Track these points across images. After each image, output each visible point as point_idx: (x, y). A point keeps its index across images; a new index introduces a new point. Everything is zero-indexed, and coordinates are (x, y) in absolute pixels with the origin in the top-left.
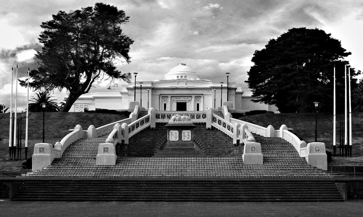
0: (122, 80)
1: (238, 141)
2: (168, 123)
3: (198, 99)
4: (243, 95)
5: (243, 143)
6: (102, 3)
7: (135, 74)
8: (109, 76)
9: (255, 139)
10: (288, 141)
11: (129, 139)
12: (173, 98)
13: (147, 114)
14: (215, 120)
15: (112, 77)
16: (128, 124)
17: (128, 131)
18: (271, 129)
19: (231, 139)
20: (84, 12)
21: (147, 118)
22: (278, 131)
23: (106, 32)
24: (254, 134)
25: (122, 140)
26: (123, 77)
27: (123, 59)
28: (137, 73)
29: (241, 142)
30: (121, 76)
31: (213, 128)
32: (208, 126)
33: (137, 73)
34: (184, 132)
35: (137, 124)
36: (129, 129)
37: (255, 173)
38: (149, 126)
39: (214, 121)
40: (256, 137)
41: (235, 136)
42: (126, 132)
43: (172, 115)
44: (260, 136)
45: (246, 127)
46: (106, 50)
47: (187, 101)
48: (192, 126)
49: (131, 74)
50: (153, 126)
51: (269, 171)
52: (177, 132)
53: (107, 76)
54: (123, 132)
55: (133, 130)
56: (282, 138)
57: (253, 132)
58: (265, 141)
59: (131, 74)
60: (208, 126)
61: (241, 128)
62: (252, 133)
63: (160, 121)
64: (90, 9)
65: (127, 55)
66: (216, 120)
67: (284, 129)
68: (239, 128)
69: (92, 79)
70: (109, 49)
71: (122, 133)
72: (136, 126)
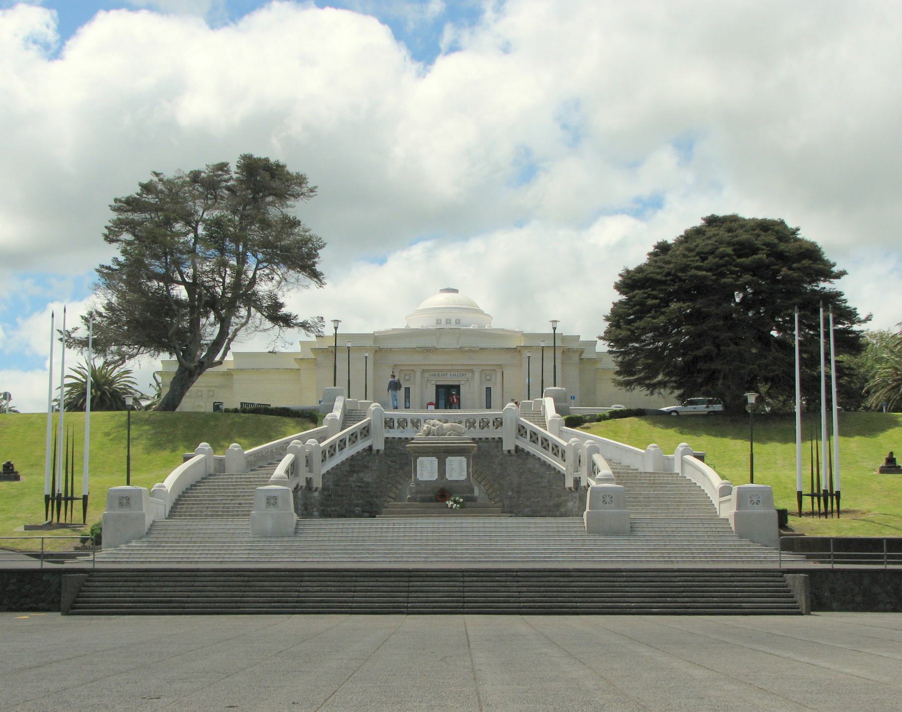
0: (303, 331)
1: (577, 481)
7: (336, 323)
10: (693, 481)
12: (427, 375)
14: (522, 431)
16: (321, 439)
17: (320, 457)
19: (561, 476)
23: (266, 224)
29: (583, 483)
32: (508, 445)
34: (450, 461)
36: (324, 452)
38: (370, 447)
39: (522, 435)
46: (265, 264)
47: (462, 382)
50: (379, 445)
52: (434, 461)
53: (268, 324)
60: (508, 445)
63: (396, 433)
64: (223, 167)
71: (307, 461)
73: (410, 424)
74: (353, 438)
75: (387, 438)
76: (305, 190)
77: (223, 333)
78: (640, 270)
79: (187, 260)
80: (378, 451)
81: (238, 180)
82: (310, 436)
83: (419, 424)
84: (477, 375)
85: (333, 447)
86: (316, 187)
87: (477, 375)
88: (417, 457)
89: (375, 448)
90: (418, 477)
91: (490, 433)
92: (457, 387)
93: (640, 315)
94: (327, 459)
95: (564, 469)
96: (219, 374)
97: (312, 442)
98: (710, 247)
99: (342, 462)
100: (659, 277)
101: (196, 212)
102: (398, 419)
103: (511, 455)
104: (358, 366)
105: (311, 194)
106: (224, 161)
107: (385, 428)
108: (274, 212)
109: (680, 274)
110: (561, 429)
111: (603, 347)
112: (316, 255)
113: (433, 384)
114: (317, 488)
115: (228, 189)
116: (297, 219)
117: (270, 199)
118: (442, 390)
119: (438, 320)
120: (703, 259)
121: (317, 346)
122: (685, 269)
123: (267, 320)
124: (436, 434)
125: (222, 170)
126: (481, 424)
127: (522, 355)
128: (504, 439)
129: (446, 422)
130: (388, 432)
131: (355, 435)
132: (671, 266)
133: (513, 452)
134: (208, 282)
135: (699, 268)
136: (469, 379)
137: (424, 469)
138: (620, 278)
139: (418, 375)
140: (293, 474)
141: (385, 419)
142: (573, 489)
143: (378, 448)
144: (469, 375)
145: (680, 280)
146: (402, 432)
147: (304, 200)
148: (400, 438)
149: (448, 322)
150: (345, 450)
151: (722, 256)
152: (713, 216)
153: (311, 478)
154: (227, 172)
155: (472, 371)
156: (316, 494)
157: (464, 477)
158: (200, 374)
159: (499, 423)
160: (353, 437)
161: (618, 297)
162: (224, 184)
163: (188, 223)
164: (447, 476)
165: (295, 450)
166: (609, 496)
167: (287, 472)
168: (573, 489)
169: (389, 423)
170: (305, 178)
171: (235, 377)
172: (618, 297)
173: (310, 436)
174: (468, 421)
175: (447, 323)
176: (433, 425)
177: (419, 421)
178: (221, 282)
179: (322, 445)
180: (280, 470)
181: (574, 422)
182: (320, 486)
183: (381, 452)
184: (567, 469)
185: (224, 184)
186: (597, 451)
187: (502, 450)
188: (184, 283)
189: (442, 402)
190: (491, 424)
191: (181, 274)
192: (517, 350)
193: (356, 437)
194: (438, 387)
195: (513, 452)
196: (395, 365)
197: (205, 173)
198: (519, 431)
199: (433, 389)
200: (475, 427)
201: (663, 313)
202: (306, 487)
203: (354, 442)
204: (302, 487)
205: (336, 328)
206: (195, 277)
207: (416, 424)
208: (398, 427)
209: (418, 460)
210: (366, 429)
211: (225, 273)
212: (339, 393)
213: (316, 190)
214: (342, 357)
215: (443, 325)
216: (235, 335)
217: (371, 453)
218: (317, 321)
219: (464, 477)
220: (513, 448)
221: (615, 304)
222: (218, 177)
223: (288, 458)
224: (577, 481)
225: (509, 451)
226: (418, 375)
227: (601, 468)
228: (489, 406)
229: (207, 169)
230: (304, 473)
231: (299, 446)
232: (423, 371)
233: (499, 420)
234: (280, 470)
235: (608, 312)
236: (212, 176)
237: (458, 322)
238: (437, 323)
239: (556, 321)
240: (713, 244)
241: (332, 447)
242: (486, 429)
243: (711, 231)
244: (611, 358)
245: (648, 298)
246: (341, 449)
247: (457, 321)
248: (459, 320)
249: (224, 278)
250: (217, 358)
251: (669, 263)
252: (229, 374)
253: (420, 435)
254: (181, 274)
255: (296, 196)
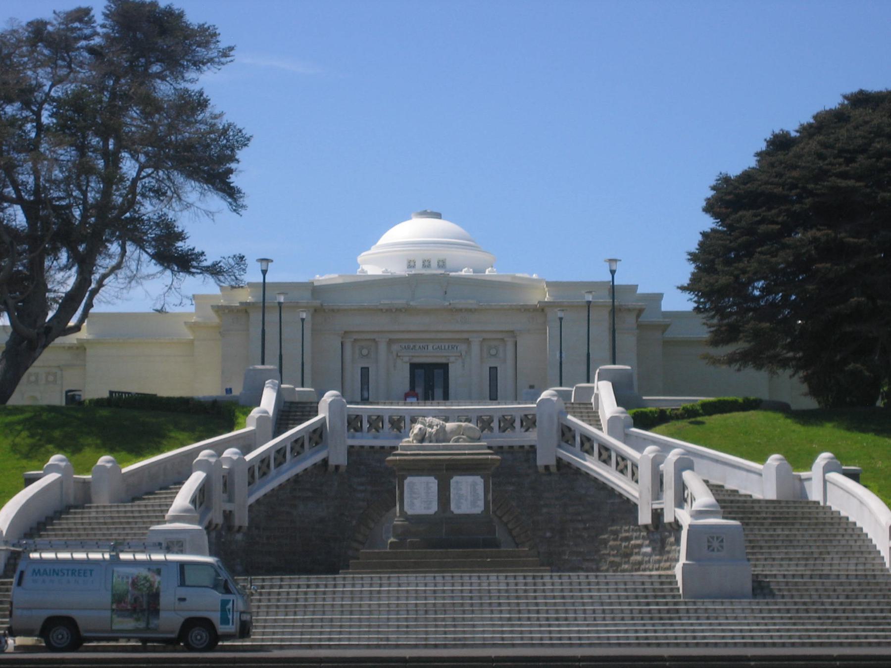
0: (210, 280)
1: (657, 515)
2: (395, 448)
3: (365, 352)
4: (669, 335)
5: (676, 521)
6: (818, 114)
7: (264, 263)
8: (159, 268)
9: (722, 507)
10: (843, 514)
11: (250, 506)
12: (395, 347)
13: (316, 413)
14: (568, 435)
15: (173, 271)
16: (247, 449)
17: (246, 478)
18: (778, 468)
19: (629, 508)
20: (60, 24)
21: (315, 431)
22: (804, 474)
23: (150, 105)
24: (716, 489)
25: (224, 511)
26: (215, 271)
27: (216, 201)
28: (272, 261)
29: (668, 518)
30: (208, 267)
31: (561, 464)
32: (544, 459)
33: (272, 261)
34: (457, 482)
35: (278, 451)
36: (251, 470)
37: (723, 631)
38: (325, 462)
39: (567, 442)
40: (724, 501)
41: (648, 496)
42: (240, 480)
43: (408, 420)
44: (741, 496)
45: (684, 464)
46: (149, 171)
48: (488, 459)
49: (244, 257)
50: (339, 458)
51: (775, 624)
52: (432, 482)
53: (152, 267)
54: (228, 482)
55: (264, 474)
56: (822, 504)
57: (713, 481)
58: (758, 513)
59: (244, 257)
60: (544, 459)
61: (668, 468)
62: (708, 486)
63: (365, 440)
64: (82, 15)
65: (228, 184)
66: (574, 437)
67: (827, 469)
68: (662, 466)
69: (96, 277)
70: (157, 168)
71: (225, 484)
72: (275, 459)
73: (387, 425)
74: (297, 447)
75: (352, 447)
76: (213, 54)
77: (83, 283)
78: (747, 177)
79: (25, 161)
80: (337, 467)
81: (106, 36)
82: (227, 444)
83: (403, 425)
84: (475, 348)
85: (266, 462)
86: (231, 49)
87: (475, 348)
88: (404, 478)
89: (332, 462)
90: (406, 508)
91: (519, 437)
92: (445, 367)
93: (748, 250)
94: (257, 481)
95: (636, 494)
96: (64, 347)
97: (230, 453)
98: (860, 141)
99: (280, 485)
100: (778, 190)
101: (40, 86)
102: (369, 417)
103: (550, 474)
104: (292, 332)
105: (223, 60)
106: (84, 5)
107: (348, 431)
108: (164, 89)
109: (811, 186)
110: (626, 431)
111: (685, 303)
112: (232, 159)
113: (407, 362)
114: (240, 527)
115: (91, 50)
116: (205, 96)
117: (156, 68)
118: (420, 372)
119: (410, 262)
120: (850, 161)
121: (222, 302)
122: (821, 175)
123: (153, 261)
124: (433, 438)
125: (80, 20)
126: (502, 425)
127: (546, 315)
128: (538, 447)
129: (447, 420)
130: (353, 437)
131: (300, 442)
132: (795, 174)
133: (553, 469)
134: (60, 199)
135: (844, 175)
136: (464, 353)
137: (414, 496)
138: (713, 193)
139: (383, 347)
140: (203, 506)
141: (349, 416)
142: (652, 529)
143: (337, 463)
144: (463, 347)
145: (811, 193)
146: (375, 438)
147: (212, 69)
148: (372, 447)
149: (426, 264)
150: (285, 466)
151: (879, 155)
152: (861, 92)
153: (230, 512)
154: (90, 21)
155: (467, 341)
156: (239, 537)
157: (479, 509)
158: (45, 346)
159: (529, 422)
160: (298, 444)
161: (709, 223)
162: (83, 43)
163: (27, 105)
164: (453, 507)
165: (204, 465)
166: (717, 538)
167: (193, 501)
168: (652, 529)
169: (354, 423)
170: (215, 35)
171: (90, 351)
172: (709, 223)
173: (227, 444)
174: (480, 419)
175: (424, 266)
176: (431, 426)
177: (401, 419)
178: (80, 199)
179: (248, 457)
180: (183, 498)
181: (645, 421)
182: (246, 524)
183: (342, 470)
184: (640, 496)
185: (83, 43)
186: (691, 467)
187: (536, 466)
188: (19, 200)
189: (419, 390)
190: (517, 424)
191: (15, 185)
192: (542, 309)
193: (302, 446)
194: (414, 367)
195: (553, 469)
196: (346, 332)
197: (53, 25)
198: (563, 434)
199: (407, 368)
200: (491, 429)
201: (784, 247)
202: (222, 525)
203: (298, 453)
204: (217, 525)
205: (264, 272)
206: (37, 190)
207: (398, 424)
208: (369, 430)
209: (406, 482)
210: (318, 432)
211: (88, 186)
212: (267, 375)
213: (232, 53)
214: (272, 317)
215: (419, 270)
216: (100, 284)
217: (326, 470)
218: (233, 263)
219: (479, 509)
220: (552, 462)
221: (704, 234)
222: (72, 33)
223: (196, 478)
224: (657, 515)
225: (547, 468)
226: (383, 347)
227: (696, 495)
228: (493, 397)
229: (56, 19)
230: (219, 505)
231: (213, 460)
232: (391, 342)
233: (530, 417)
234: (183, 498)
235: (694, 247)
236: (63, 29)
237: (442, 264)
238: (409, 266)
239: (615, 260)
240: (864, 137)
241: (264, 460)
242: (509, 431)
243: (858, 114)
244: (700, 318)
245: (760, 222)
246: (279, 464)
247: (427, 264)
248: (444, 262)
249: (84, 193)
250: (72, 323)
251: (794, 167)
252: (81, 348)
253: (409, 442)
254: (15, 185)
255: (198, 64)
